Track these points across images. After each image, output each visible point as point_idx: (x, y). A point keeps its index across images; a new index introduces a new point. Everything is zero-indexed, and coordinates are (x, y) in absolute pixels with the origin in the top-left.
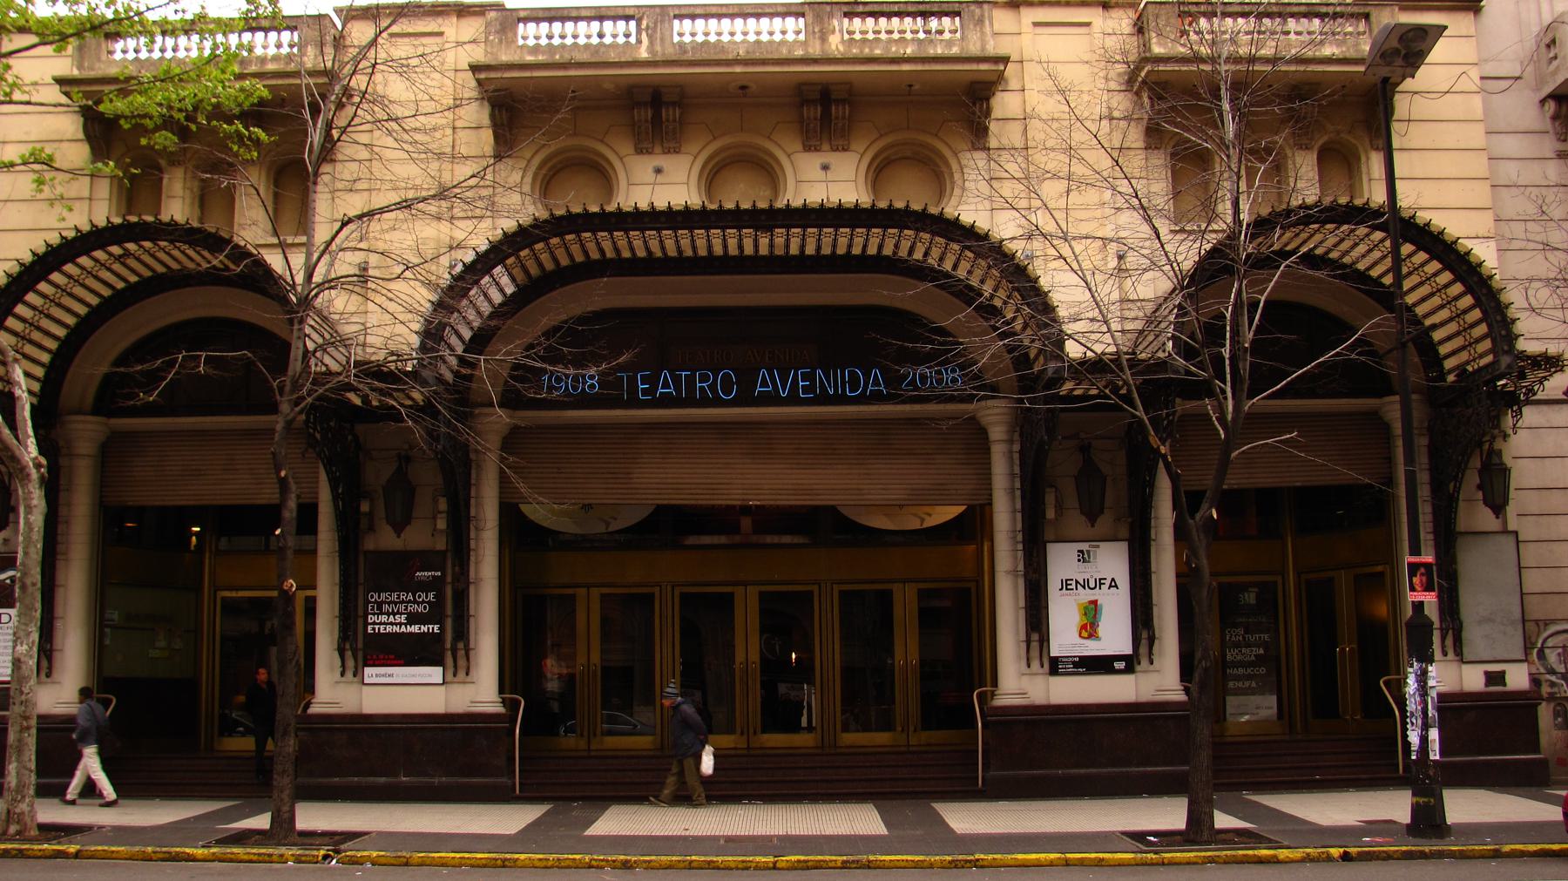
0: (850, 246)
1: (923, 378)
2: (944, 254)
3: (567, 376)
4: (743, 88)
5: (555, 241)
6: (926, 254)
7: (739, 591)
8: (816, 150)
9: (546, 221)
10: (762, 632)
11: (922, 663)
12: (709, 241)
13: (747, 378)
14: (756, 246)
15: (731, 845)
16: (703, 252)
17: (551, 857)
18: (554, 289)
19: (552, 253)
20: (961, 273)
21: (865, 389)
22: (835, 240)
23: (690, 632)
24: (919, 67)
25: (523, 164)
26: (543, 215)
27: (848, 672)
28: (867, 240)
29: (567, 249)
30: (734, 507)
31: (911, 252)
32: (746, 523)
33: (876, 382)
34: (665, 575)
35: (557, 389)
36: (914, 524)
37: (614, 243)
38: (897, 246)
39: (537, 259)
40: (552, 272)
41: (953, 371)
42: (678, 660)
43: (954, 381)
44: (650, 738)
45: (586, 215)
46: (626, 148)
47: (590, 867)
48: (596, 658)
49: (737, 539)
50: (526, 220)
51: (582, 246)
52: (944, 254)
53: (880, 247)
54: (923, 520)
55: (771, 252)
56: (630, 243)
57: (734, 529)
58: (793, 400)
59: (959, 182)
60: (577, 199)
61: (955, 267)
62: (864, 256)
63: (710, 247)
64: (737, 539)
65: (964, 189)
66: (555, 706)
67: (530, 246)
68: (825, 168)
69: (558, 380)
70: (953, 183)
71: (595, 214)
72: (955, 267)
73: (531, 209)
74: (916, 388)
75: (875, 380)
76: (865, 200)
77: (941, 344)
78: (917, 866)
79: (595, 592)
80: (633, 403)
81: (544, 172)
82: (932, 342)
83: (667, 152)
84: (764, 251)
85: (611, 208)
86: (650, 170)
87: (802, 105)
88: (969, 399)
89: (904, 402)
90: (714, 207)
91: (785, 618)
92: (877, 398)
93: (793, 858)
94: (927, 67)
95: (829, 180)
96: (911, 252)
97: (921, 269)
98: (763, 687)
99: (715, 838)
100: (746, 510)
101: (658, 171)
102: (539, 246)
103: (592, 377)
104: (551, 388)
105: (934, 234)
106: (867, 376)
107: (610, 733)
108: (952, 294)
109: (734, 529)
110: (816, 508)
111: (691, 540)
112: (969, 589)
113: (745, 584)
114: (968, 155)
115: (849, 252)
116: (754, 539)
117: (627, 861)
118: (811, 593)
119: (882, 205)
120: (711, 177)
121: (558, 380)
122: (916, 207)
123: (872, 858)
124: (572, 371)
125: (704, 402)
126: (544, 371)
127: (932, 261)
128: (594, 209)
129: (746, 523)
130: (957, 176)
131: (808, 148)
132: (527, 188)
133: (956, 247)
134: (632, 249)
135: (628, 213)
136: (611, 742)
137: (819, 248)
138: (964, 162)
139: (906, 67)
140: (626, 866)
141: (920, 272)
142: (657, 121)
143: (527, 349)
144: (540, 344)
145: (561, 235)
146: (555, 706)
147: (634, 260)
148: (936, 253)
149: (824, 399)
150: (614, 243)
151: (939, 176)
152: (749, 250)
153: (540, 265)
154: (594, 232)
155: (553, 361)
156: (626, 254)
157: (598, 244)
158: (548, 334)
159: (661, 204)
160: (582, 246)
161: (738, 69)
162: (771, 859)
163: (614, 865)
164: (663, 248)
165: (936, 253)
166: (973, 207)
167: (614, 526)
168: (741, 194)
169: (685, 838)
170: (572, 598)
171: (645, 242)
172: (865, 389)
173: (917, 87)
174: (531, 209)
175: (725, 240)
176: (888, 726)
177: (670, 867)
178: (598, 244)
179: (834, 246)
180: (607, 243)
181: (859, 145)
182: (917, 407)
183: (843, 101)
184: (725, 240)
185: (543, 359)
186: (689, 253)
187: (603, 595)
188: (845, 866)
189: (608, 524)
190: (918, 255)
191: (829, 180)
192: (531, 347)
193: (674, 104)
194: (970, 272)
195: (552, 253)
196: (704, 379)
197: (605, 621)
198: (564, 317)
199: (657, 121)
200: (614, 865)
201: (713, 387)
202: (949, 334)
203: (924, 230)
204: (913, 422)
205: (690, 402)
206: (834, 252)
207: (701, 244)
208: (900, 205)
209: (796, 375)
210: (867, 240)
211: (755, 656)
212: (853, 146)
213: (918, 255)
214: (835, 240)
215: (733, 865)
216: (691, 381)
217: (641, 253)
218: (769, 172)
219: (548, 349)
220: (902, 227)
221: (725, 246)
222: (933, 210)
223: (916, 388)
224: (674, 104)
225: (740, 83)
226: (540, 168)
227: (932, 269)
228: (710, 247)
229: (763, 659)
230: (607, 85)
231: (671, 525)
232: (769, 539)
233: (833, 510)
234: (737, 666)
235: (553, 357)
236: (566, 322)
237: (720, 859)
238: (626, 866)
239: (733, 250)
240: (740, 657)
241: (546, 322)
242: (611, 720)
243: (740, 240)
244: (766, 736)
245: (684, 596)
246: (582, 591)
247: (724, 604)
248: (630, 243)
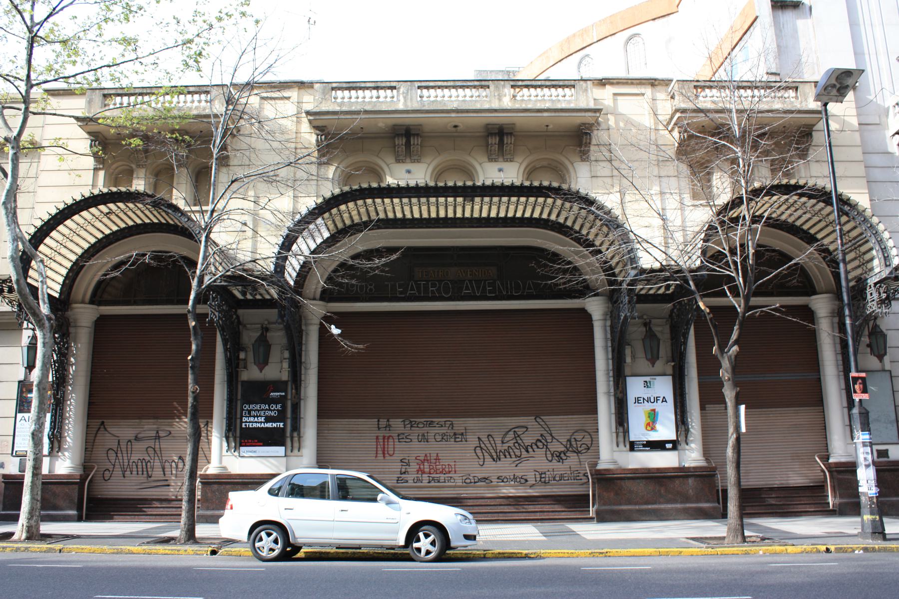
4: (456, 126)
68: (409, 172)
120: (530, 172)
137: (498, 214)
173: (551, 127)
181: (519, 159)
201: (438, 290)
225: (454, 124)
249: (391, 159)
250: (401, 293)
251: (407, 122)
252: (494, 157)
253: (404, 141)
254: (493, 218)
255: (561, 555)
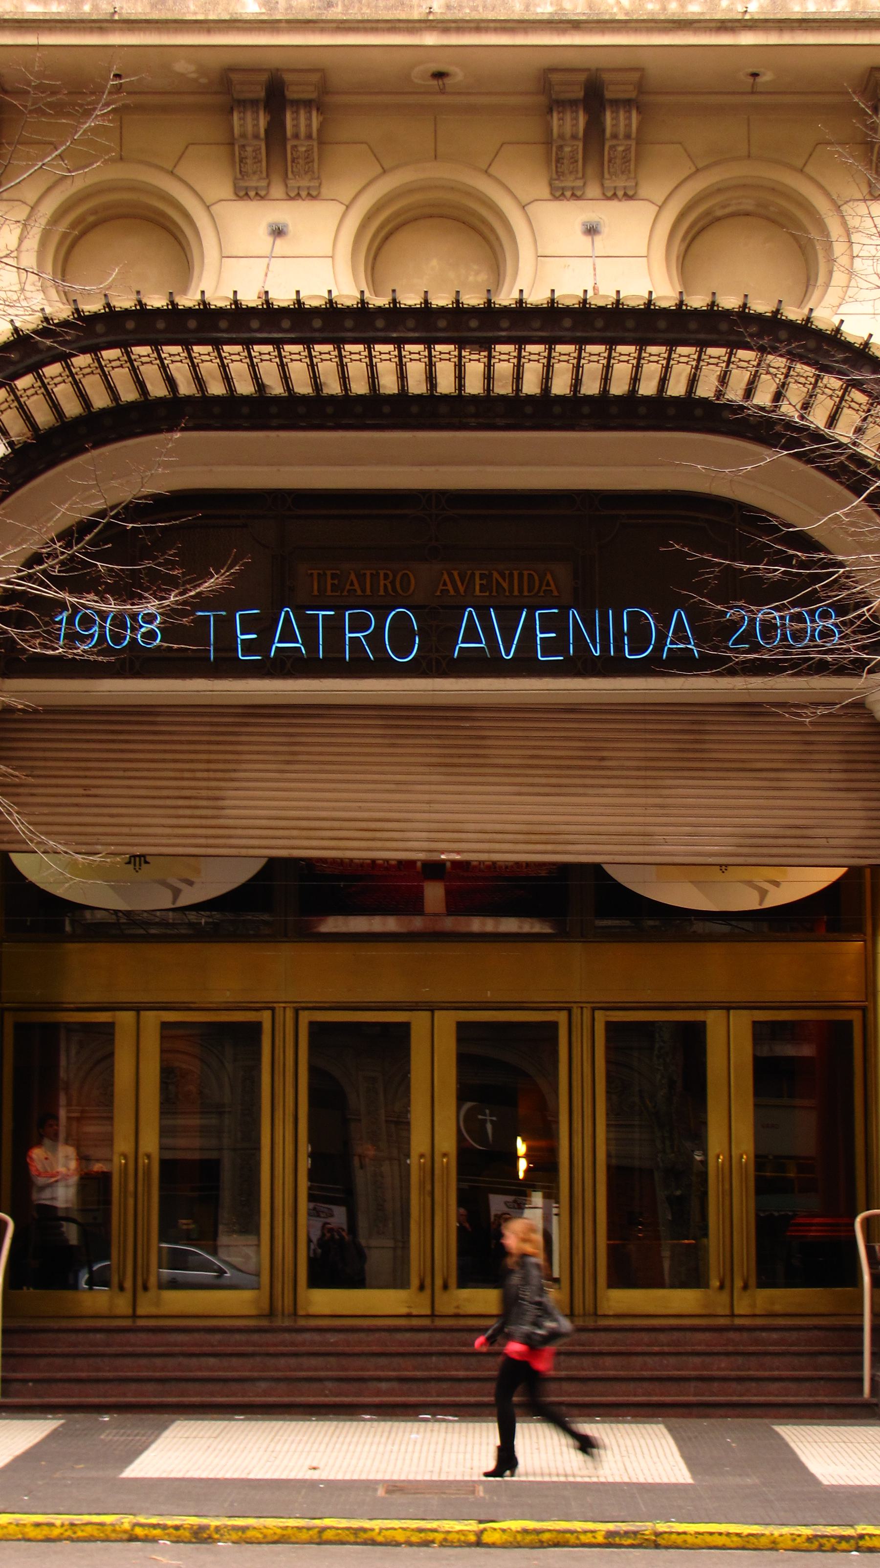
0: (635, 380)
1: (768, 628)
2: (811, 395)
3: (103, 615)
4: (439, 75)
5: (82, 361)
6: (778, 396)
7: (419, 1021)
8: (575, 197)
9: (65, 324)
10: (461, 1097)
11: (760, 1160)
12: (371, 366)
13: (439, 623)
14: (460, 377)
15: (397, 1497)
16: (360, 387)
17: (58, 1520)
18: (83, 450)
19: (76, 384)
20: (843, 432)
21: (659, 648)
22: (608, 368)
23: (327, 1099)
24: (773, 39)
25: (22, 213)
26: (61, 311)
27: (620, 1177)
28: (667, 368)
29: (105, 377)
30: (411, 863)
31: (749, 393)
32: (434, 894)
33: (680, 636)
34: (287, 988)
35: (83, 639)
36: (748, 901)
37: (194, 367)
38: (723, 379)
39: (49, 396)
40: (78, 420)
41: (825, 615)
42: (304, 1148)
43: (826, 634)
44: (247, 1295)
45: (142, 313)
46: (218, 187)
47: (133, 1538)
48: (150, 1143)
49: (417, 923)
50: (29, 322)
51: (134, 371)
52: (811, 395)
53: (693, 381)
54: (763, 893)
55: (488, 388)
56: (223, 367)
57: (411, 904)
58: (525, 665)
59: (843, 260)
60: (125, 282)
61: (832, 421)
62: (632, 398)
63: (373, 377)
64: (417, 923)
65: (851, 273)
66: (72, 1233)
67: (35, 368)
68: (591, 230)
69: (87, 622)
70: (831, 260)
71: (158, 311)
72: (832, 421)
73: (37, 300)
74: (756, 648)
75: (677, 633)
76: (666, 294)
77: (802, 565)
78: (748, 1544)
79: (152, 1020)
80: (227, 666)
81: (62, 228)
82: (786, 561)
83: (294, 196)
84: (474, 386)
85: (188, 300)
86: (262, 231)
87: (550, 111)
88: (857, 668)
89: (732, 672)
90: (382, 301)
91: (505, 1074)
92: (682, 664)
93: (516, 1525)
94: (787, 39)
95: (594, 250)
96: (749, 393)
97: (770, 423)
98: (461, 1202)
99: (368, 1486)
100: (434, 870)
101: (278, 232)
102: (52, 370)
103: (150, 618)
104: (73, 638)
105: (793, 356)
106: (663, 621)
107: (174, 1285)
108: (825, 471)
109: (411, 904)
110: (564, 869)
111: (332, 924)
112: (849, 1024)
113: (431, 1008)
114: (862, 208)
115: (633, 390)
116: (449, 924)
117: (203, 1528)
118: (554, 1025)
119: (697, 302)
120: (379, 243)
121: (87, 622)
122: (761, 306)
123: (661, 1527)
124: (112, 607)
125: (360, 667)
126: (62, 605)
127: (789, 410)
128: (157, 301)
129: (434, 894)
130: (839, 248)
131: (558, 194)
132: (29, 260)
133: (833, 382)
134: (227, 379)
135: (221, 311)
136: (178, 1301)
137: (577, 382)
138: (853, 222)
139: (747, 39)
140: (200, 1536)
141: (766, 430)
142: (275, 135)
143: (28, 564)
144: (51, 555)
145: (94, 350)
146: (72, 1233)
147: (292, 400)
148: (795, 394)
149: (582, 666)
150: (194, 367)
151: (807, 251)
152: (446, 385)
153: (55, 406)
154: (187, 345)
155: (77, 586)
156: (216, 388)
157: (164, 368)
158: (68, 536)
159: (283, 297)
160: (134, 371)
161: (430, 39)
162: (472, 1526)
163: (177, 1536)
164: (286, 378)
165: (795, 394)
166: (868, 308)
167: (190, 897)
168: (432, 279)
169: (312, 1485)
170: (107, 1031)
171: (253, 366)
172: (659, 648)
173: (767, 77)
174: (37, 300)
175: (401, 365)
176: (693, 1277)
177: (282, 1539)
178: (164, 368)
179: (606, 379)
180: (181, 368)
181: (655, 188)
182: (756, 682)
183: (628, 104)
184: (401, 365)
185: (59, 583)
186: (333, 388)
187: (165, 1025)
188: (612, 1541)
189: (176, 893)
190: (763, 398)
191: (594, 250)
192: (36, 559)
193: (308, 104)
194: (859, 430)
195: (76, 384)
196: (359, 624)
197: (168, 1074)
198: (98, 505)
199: (275, 135)
200: (177, 1536)
201: (376, 640)
202: (817, 547)
203: (774, 351)
204: (751, 710)
205: (333, 667)
206: (605, 390)
207: (299, 371)
208: (730, 302)
209: (530, 619)
210: (667, 368)
211: (447, 1143)
212: (643, 192)
213: (763, 398)
214: (608, 368)
215: (400, 1537)
216: (334, 628)
217: (245, 387)
218: (481, 233)
219: (70, 563)
220: (734, 345)
221: (402, 376)
222: (793, 313)
223: (756, 648)
224: (308, 104)
225: (435, 67)
226: (55, 219)
227: (789, 425)
228: (373, 377)
229: (463, 1151)
230: (182, 66)
231: (294, 896)
232: (477, 924)
233: (597, 869)
234: (414, 1161)
235: (77, 579)
236: (102, 514)
237: (376, 1524)
238: (200, 1536)
239: (389, 384)
240: (419, 1143)
241: (67, 513)
242: (178, 1260)
243: (431, 365)
244: (466, 1293)
245: (318, 1030)
246: (125, 1018)
247: (392, 1042)
248: (223, 367)
249: (532, 184)
250: (248, 646)
251: (275, 60)
252: (253, 182)
253: (263, 122)
254: (646, 400)
255: (720, 1541)
